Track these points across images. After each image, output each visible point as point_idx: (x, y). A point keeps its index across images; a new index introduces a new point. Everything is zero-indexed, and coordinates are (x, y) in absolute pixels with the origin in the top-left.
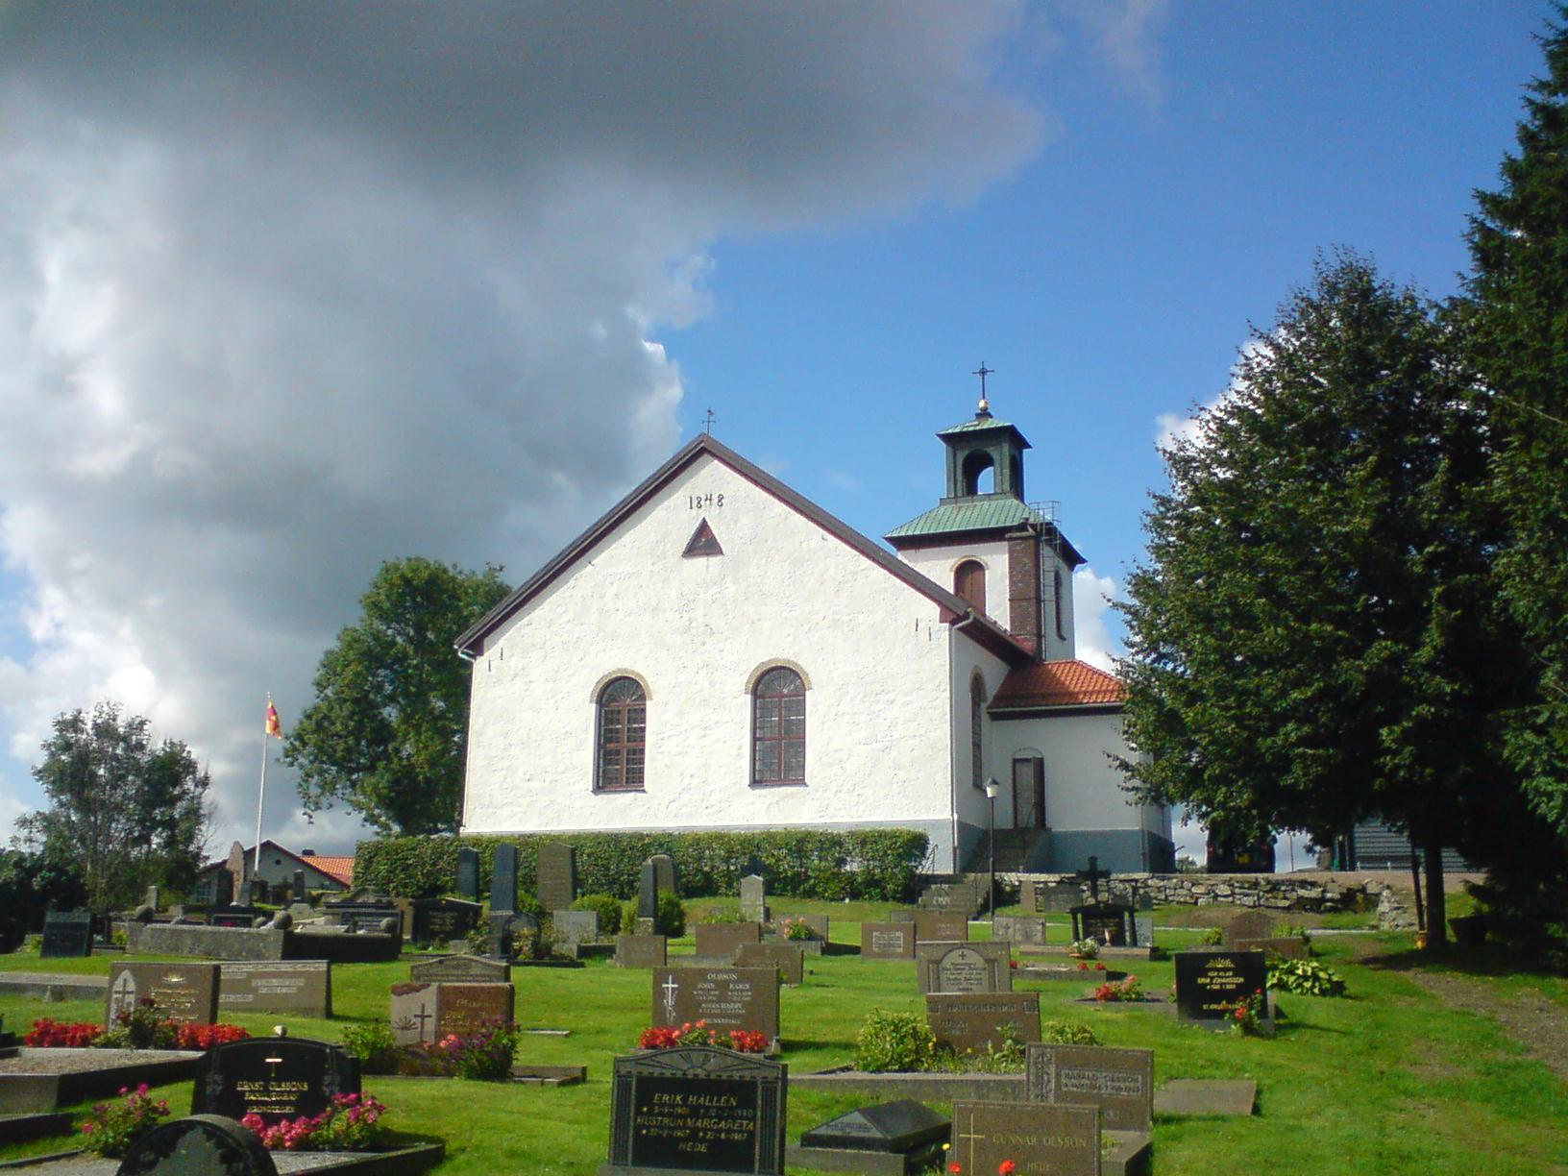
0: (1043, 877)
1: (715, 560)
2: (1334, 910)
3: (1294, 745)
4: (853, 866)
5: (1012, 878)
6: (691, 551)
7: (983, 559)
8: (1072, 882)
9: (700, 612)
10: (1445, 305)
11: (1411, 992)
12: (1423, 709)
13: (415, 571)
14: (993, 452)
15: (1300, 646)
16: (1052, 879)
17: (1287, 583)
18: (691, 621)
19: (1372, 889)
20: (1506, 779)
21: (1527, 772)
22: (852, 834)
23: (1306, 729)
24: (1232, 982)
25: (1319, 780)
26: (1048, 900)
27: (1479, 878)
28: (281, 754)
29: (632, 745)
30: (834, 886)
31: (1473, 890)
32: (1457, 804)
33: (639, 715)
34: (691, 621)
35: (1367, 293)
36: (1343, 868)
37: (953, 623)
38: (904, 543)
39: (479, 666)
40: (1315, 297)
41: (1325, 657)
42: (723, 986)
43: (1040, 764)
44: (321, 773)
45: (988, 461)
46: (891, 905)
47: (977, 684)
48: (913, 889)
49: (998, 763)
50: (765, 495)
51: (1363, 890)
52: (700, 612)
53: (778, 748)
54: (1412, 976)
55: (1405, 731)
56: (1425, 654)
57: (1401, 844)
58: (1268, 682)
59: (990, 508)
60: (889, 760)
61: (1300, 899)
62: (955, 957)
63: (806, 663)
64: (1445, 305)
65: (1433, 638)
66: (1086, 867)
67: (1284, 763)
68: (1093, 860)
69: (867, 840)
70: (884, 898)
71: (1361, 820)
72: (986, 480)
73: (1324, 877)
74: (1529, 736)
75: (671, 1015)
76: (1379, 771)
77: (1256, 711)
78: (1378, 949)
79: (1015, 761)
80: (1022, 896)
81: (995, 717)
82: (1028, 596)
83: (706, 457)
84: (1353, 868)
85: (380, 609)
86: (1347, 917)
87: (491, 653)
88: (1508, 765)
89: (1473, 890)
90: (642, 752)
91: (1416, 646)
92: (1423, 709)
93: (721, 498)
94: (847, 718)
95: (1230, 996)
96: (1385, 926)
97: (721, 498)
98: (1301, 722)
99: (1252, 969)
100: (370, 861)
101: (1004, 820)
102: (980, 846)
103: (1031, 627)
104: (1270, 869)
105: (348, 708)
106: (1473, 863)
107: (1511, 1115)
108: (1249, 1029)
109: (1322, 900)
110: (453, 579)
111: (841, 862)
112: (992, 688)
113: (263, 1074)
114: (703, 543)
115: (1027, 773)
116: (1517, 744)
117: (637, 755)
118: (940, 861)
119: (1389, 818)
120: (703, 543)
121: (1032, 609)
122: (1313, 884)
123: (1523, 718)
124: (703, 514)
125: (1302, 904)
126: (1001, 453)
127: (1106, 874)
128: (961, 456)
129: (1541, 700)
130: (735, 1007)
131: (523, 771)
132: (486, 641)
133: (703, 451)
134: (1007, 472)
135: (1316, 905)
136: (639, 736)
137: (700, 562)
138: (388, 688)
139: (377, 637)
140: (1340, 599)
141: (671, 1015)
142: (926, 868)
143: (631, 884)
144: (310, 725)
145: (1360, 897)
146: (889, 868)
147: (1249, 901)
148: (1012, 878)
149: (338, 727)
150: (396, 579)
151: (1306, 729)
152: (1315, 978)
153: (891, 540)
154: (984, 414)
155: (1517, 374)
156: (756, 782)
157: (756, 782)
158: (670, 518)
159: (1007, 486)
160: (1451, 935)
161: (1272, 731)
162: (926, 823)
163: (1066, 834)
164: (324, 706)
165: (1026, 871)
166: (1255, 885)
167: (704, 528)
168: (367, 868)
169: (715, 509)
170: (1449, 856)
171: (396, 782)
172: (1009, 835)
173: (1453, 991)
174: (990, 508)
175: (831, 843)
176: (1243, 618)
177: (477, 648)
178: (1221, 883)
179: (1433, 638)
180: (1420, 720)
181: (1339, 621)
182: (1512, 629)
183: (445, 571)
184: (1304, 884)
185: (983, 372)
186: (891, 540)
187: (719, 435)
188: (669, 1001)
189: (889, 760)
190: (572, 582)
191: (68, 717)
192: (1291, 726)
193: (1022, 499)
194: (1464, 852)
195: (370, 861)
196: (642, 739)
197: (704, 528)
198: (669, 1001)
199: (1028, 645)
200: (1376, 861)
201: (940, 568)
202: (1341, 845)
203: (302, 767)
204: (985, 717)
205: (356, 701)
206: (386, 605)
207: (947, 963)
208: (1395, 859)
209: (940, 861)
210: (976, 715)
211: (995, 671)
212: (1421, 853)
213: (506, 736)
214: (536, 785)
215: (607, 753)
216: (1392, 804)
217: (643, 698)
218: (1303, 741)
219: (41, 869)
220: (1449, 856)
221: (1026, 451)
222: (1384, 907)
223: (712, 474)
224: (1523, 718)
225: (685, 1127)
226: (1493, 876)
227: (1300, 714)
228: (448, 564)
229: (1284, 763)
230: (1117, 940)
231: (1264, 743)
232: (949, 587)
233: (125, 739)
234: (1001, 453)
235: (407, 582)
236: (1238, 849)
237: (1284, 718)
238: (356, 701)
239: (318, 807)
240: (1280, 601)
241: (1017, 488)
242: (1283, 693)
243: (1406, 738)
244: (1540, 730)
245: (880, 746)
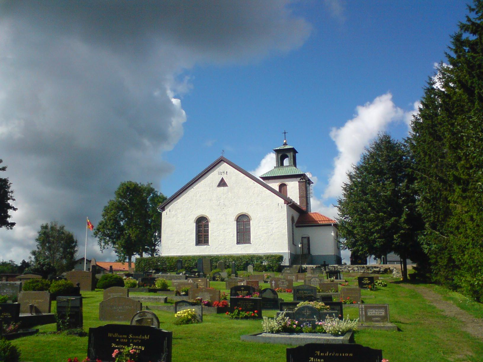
0: (312, 266)
3: (377, 238)
4: (265, 263)
5: (304, 266)
6: (219, 185)
7: (286, 183)
8: (319, 267)
9: (222, 201)
10: (406, 139)
11: (400, 287)
12: (402, 231)
13: (130, 185)
14: (288, 154)
15: (377, 217)
16: (314, 266)
17: (374, 204)
19: (391, 269)
20: (418, 245)
21: (422, 244)
22: (265, 256)
23: (379, 235)
24: (368, 282)
25: (382, 245)
26: (314, 272)
27: (415, 265)
28: (93, 234)
29: (205, 234)
30: (261, 268)
31: (414, 268)
32: (410, 250)
33: (207, 226)
35: (389, 142)
36: (384, 264)
38: (264, 178)
39: (164, 214)
40: (378, 142)
41: (382, 220)
42: (283, 282)
43: (308, 238)
44: (105, 239)
45: (287, 157)
46: (275, 273)
47: (293, 219)
48: (280, 269)
49: (298, 239)
50: (238, 172)
51: (389, 269)
52: (222, 201)
53: (243, 233)
54: (401, 285)
55: (399, 236)
56: (402, 220)
57: (397, 257)
58: (370, 225)
59: (288, 169)
60: (272, 237)
61: (374, 271)
62: (313, 279)
63: (250, 214)
64: (406, 139)
65: (404, 217)
66: (323, 263)
67: (374, 241)
68: (325, 262)
69: (268, 257)
70: (273, 271)
71: (389, 252)
72: (286, 162)
73: (382, 265)
74: (423, 237)
75: (274, 287)
76: (393, 243)
77: (368, 231)
78: (393, 281)
79: (302, 238)
80: (308, 270)
81: (297, 227)
82: (305, 195)
84: (386, 264)
85: (121, 195)
86: (386, 275)
87: (167, 210)
88: (419, 242)
89: (414, 268)
90: (208, 235)
91: (400, 218)
92: (402, 231)
95: (368, 284)
96: (395, 277)
98: (377, 234)
99: (372, 280)
100: (139, 262)
101: (299, 252)
102: (295, 259)
103: (305, 204)
104: (366, 264)
105: (112, 222)
106: (414, 261)
108: (371, 290)
109: (380, 271)
110: (140, 187)
111: (262, 263)
112: (296, 219)
113: (241, 290)
114: (222, 183)
115: (305, 241)
116: (421, 238)
117: (207, 236)
118: (286, 262)
119: (396, 252)
120: (222, 183)
121: (305, 200)
122: (377, 267)
123: (422, 233)
124: (222, 176)
125: (375, 272)
126: (291, 155)
127: (328, 265)
128: (280, 155)
129: (425, 229)
130: (286, 286)
131: (175, 239)
132: (166, 207)
133: (222, 160)
134: (292, 160)
135: (378, 272)
136: (207, 231)
137: (222, 188)
138: (122, 216)
139: (120, 202)
140: (384, 208)
141: (274, 287)
142: (283, 264)
144: (101, 226)
145: (389, 270)
146: (274, 263)
147: (362, 271)
148: (304, 266)
149: (109, 227)
150: (125, 187)
151: (379, 235)
152: (381, 283)
153: (261, 178)
154: (285, 144)
155: (419, 168)
156: (238, 243)
157: (238, 243)
158: (214, 177)
159: (292, 164)
160: (408, 277)
161: (371, 235)
162: (282, 253)
164: (104, 221)
165: (307, 264)
166: (364, 267)
167: (222, 179)
168: (139, 264)
169: (225, 175)
170: (408, 261)
171: (126, 242)
172: (302, 256)
173: (408, 287)
174: (288, 169)
175: (259, 258)
176: (364, 211)
177: (163, 209)
178: (355, 267)
179: (404, 217)
180: (401, 233)
181: (385, 213)
182: (420, 215)
183: (138, 185)
184: (375, 267)
185: (285, 133)
186: (261, 178)
187: (226, 156)
188: (273, 285)
189: (272, 237)
191: (44, 225)
192: (375, 234)
193: (295, 166)
194: (412, 260)
195: (139, 262)
196: (208, 232)
197: (222, 179)
198: (273, 285)
199: (304, 208)
200: (392, 262)
201: (275, 185)
202: (383, 258)
203: (99, 238)
204: (294, 227)
205: (114, 220)
206: (122, 194)
207: (312, 280)
208: (396, 262)
209: (286, 262)
210: (293, 226)
211: (296, 215)
212: (402, 260)
213: (172, 231)
214: (180, 243)
215: (199, 236)
216: (397, 250)
217: (208, 222)
218: (379, 238)
219: (45, 265)
220: (408, 261)
221: (297, 154)
222: (394, 272)
223: (224, 166)
224: (422, 233)
226: (418, 265)
227: (377, 232)
228: (138, 183)
229: (374, 241)
230: (337, 278)
231: (370, 238)
232: (278, 190)
233: (59, 231)
234: (291, 155)
235: (128, 188)
236: (358, 259)
237: (373, 233)
238: (114, 220)
239: (104, 248)
240: (373, 209)
241: (295, 164)
242: (374, 228)
243: (399, 237)
244: (425, 235)
245: (270, 234)
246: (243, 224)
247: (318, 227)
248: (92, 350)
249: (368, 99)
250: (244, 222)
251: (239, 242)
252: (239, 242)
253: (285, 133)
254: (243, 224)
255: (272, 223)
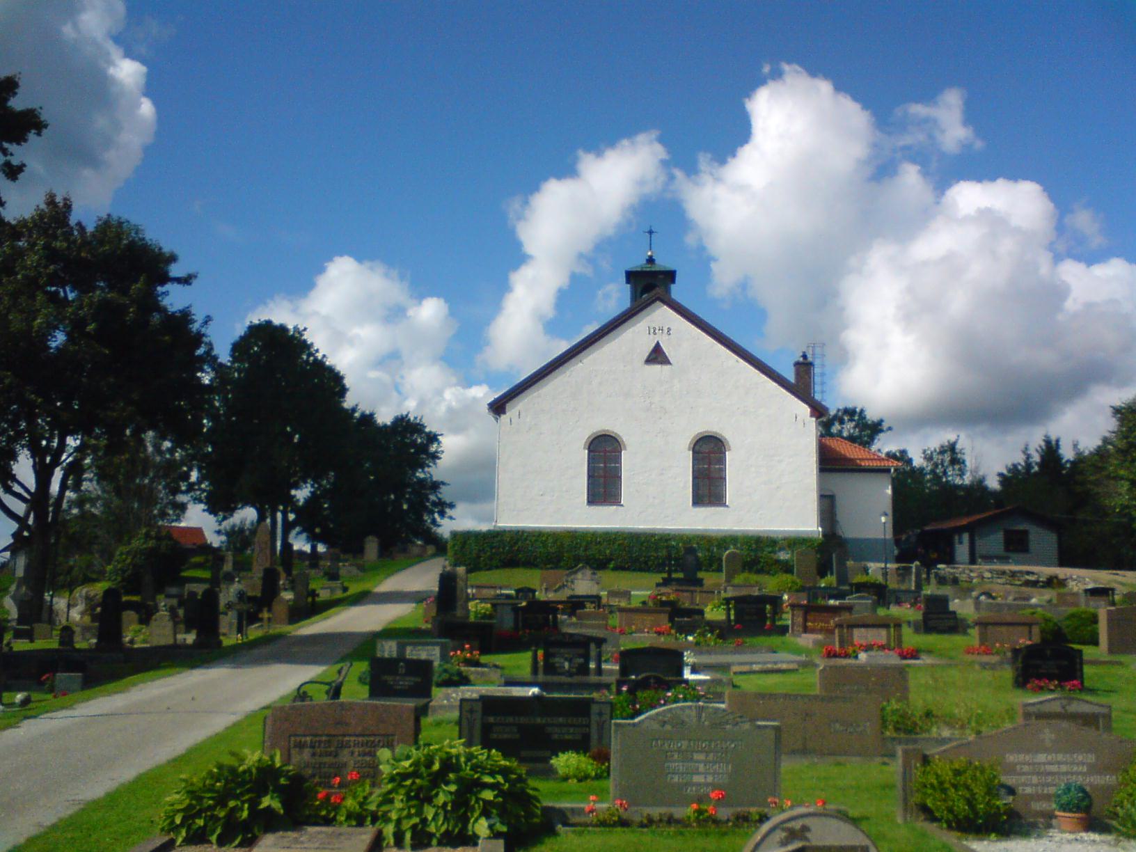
1: (666, 368)
2: (1043, 587)
6: (650, 361)
18: (651, 403)
22: (784, 539)
34: (651, 403)
37: (817, 418)
53: (708, 483)
63: (727, 434)
83: (658, 303)
93: (669, 329)
94: (753, 469)
97: (669, 329)
107: (725, 834)
114: (657, 356)
120: (657, 356)
125: (1028, 583)
132: (508, 406)
135: (1034, 584)
143: (646, 563)
156: (591, 501)
157: (591, 501)
158: (638, 337)
163: (857, 540)
169: (665, 337)
185: (651, 232)
189: (775, 494)
190: (568, 373)
225: (408, 757)
246: (709, 457)
247: (856, 474)
248: (524, 754)
249: (602, 138)
250: (605, 452)
251: (698, 500)
252: (698, 500)
253: (651, 232)
254: (709, 457)
255: (780, 461)
